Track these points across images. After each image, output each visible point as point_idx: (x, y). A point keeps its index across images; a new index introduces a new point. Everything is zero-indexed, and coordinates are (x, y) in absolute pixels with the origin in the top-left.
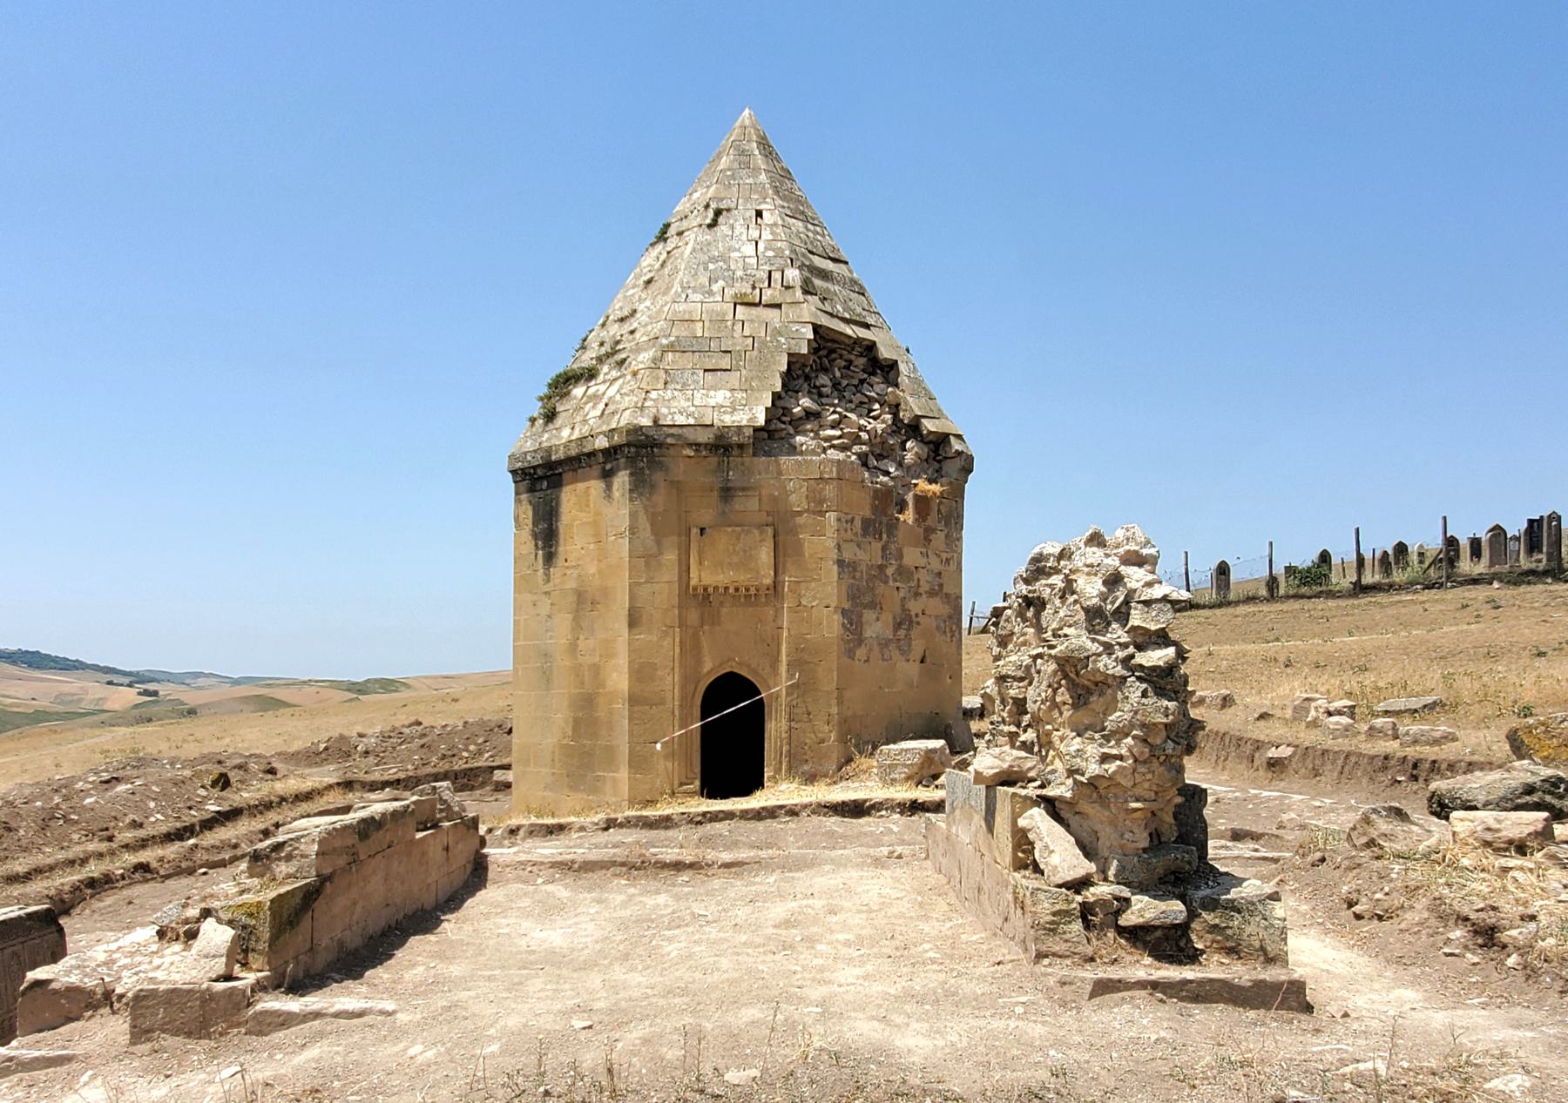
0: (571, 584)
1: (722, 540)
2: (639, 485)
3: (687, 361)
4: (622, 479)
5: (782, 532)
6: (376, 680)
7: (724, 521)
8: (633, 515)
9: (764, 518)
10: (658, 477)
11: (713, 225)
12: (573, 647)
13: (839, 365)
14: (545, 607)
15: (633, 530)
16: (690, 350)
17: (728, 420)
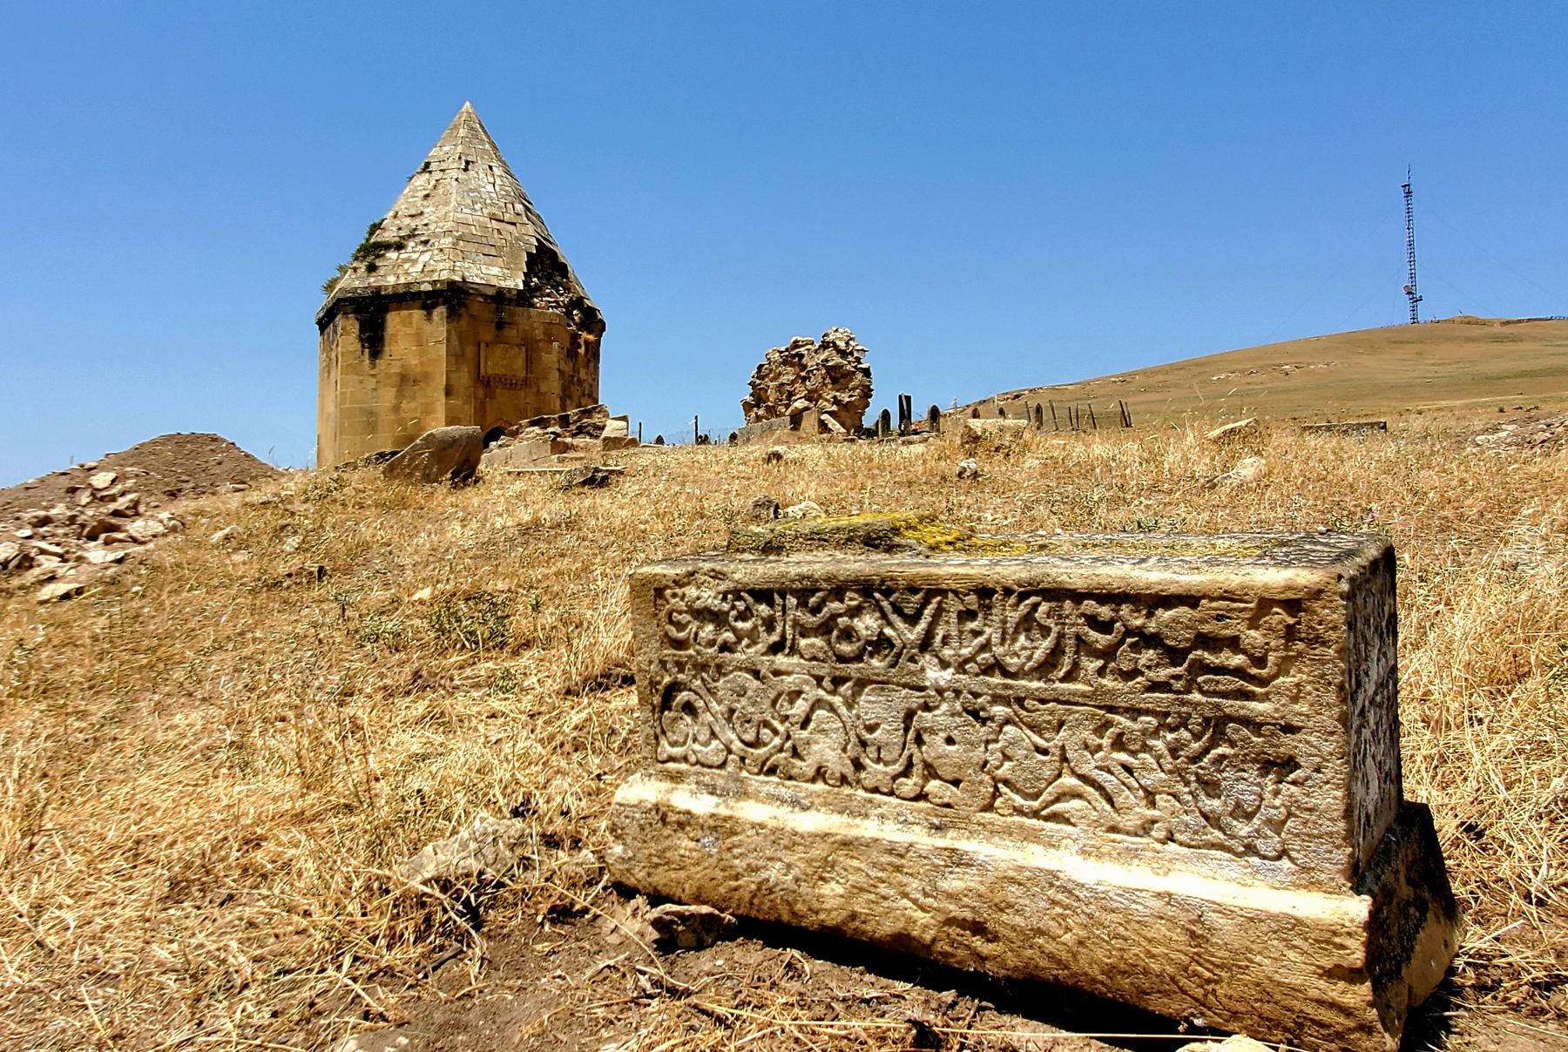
0: (396, 369)
1: (498, 351)
2: (452, 315)
3: (470, 247)
4: (440, 312)
5: (530, 347)
6: (170, 438)
7: (498, 340)
8: (448, 331)
9: (519, 341)
10: (463, 311)
11: (466, 170)
12: (396, 409)
13: (545, 264)
14: (371, 383)
15: (448, 339)
16: (464, 240)
17: (503, 284)
